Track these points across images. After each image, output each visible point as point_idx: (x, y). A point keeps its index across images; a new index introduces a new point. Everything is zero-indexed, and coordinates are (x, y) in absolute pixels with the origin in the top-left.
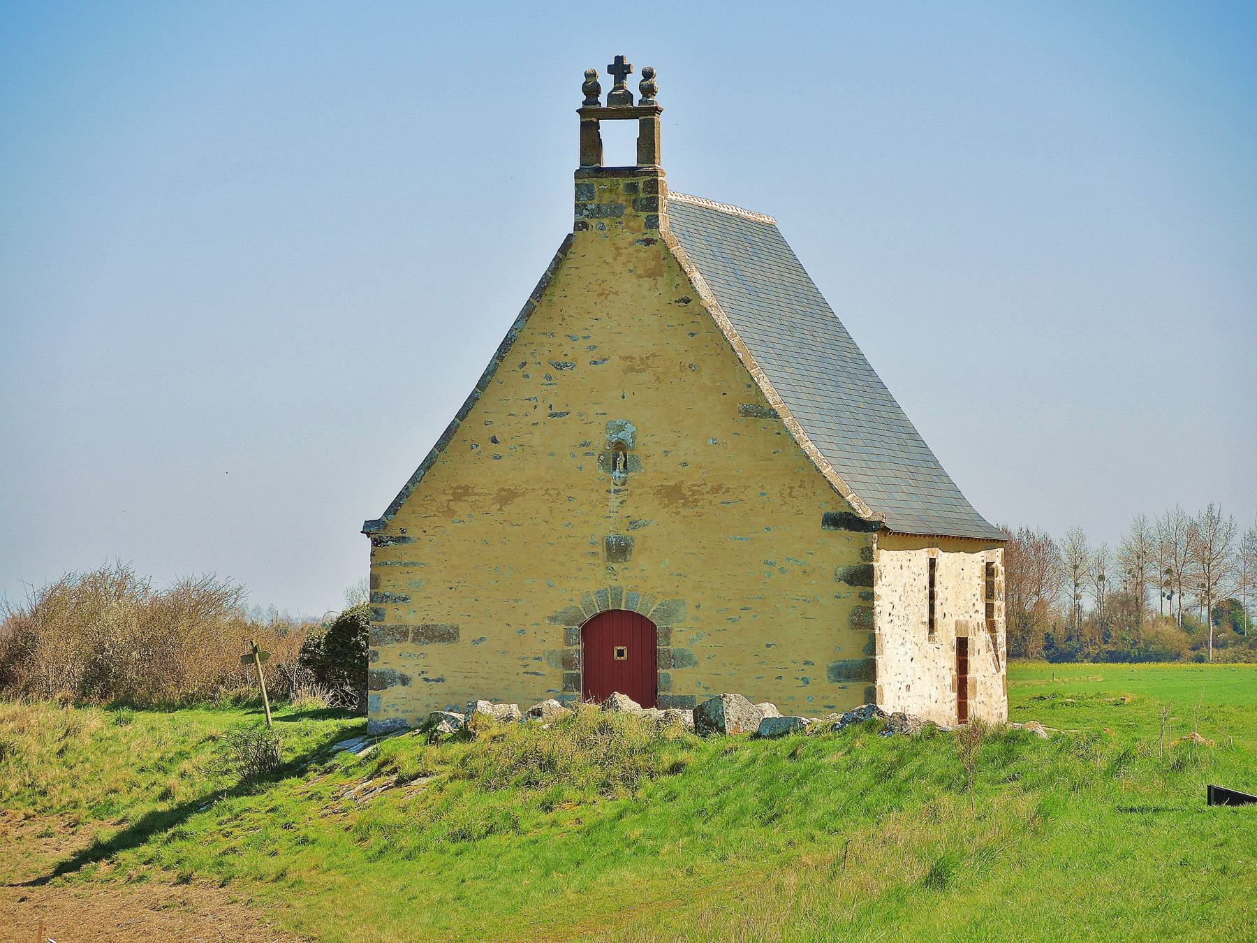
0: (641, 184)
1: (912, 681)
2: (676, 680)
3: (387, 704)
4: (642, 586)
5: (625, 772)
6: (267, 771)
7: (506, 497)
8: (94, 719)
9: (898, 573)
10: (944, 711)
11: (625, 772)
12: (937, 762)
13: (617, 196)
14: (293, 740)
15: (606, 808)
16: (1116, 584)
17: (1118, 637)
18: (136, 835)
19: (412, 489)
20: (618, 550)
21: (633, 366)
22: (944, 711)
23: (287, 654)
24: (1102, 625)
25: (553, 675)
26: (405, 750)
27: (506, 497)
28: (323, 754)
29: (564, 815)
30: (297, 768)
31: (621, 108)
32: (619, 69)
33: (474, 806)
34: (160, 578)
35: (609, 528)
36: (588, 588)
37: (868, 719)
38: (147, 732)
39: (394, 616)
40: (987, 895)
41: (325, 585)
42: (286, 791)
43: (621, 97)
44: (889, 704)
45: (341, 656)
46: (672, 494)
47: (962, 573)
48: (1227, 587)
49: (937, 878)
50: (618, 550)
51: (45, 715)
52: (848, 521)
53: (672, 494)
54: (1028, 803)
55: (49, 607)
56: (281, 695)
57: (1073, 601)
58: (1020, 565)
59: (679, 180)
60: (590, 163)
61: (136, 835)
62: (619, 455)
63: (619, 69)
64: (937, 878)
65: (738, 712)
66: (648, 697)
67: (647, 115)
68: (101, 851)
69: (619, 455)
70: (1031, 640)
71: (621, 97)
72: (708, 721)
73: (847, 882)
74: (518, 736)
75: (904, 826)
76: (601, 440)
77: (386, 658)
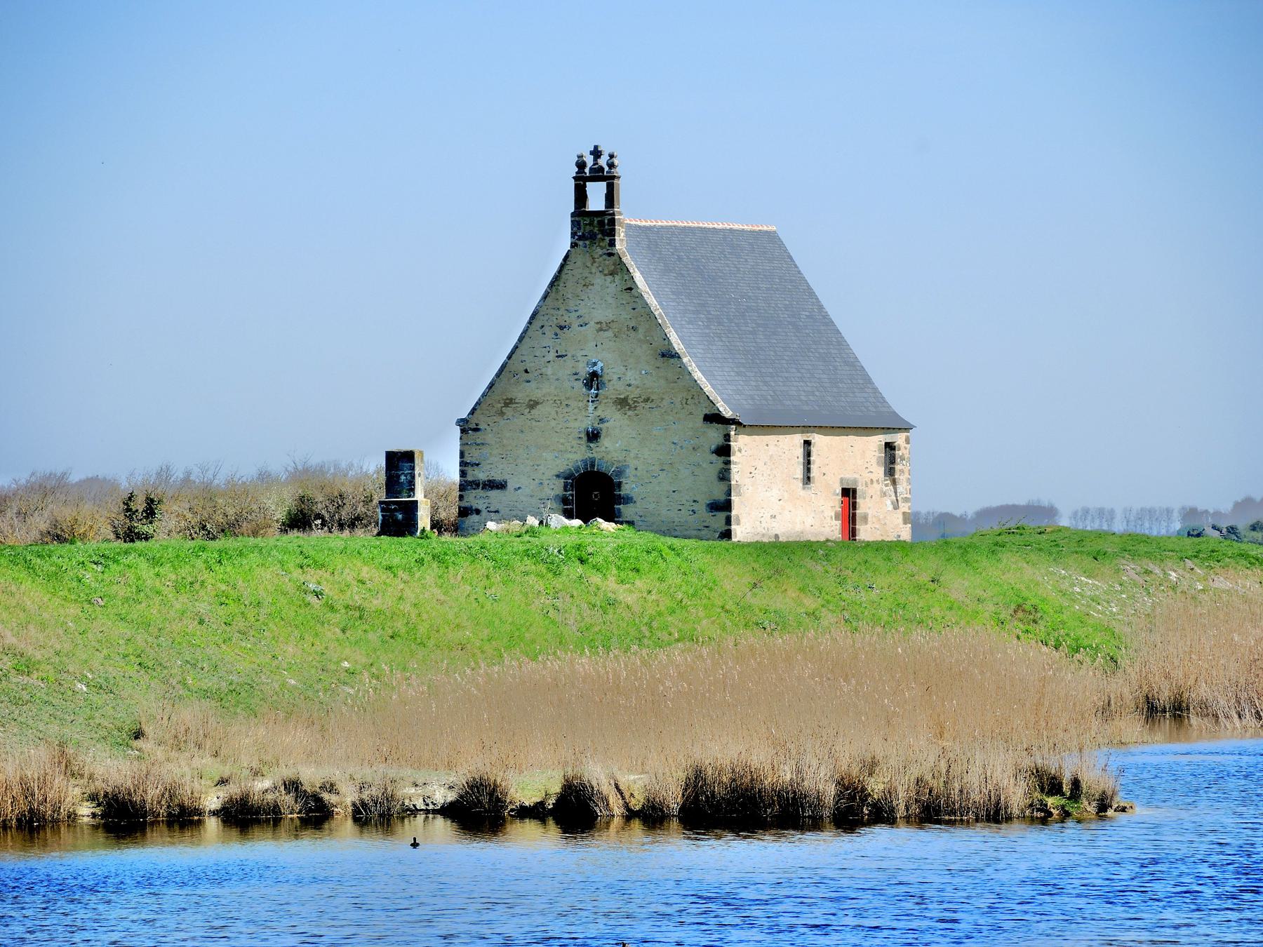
4: (609, 452)
7: (533, 405)
13: (593, 229)
21: (602, 327)
31: (598, 175)
32: (596, 153)
35: (588, 423)
36: (575, 456)
43: (594, 171)
46: (623, 403)
50: (593, 436)
52: (714, 418)
53: (623, 403)
59: (626, 216)
62: (593, 379)
63: (596, 153)
69: (593, 379)
71: (594, 171)
76: (584, 371)
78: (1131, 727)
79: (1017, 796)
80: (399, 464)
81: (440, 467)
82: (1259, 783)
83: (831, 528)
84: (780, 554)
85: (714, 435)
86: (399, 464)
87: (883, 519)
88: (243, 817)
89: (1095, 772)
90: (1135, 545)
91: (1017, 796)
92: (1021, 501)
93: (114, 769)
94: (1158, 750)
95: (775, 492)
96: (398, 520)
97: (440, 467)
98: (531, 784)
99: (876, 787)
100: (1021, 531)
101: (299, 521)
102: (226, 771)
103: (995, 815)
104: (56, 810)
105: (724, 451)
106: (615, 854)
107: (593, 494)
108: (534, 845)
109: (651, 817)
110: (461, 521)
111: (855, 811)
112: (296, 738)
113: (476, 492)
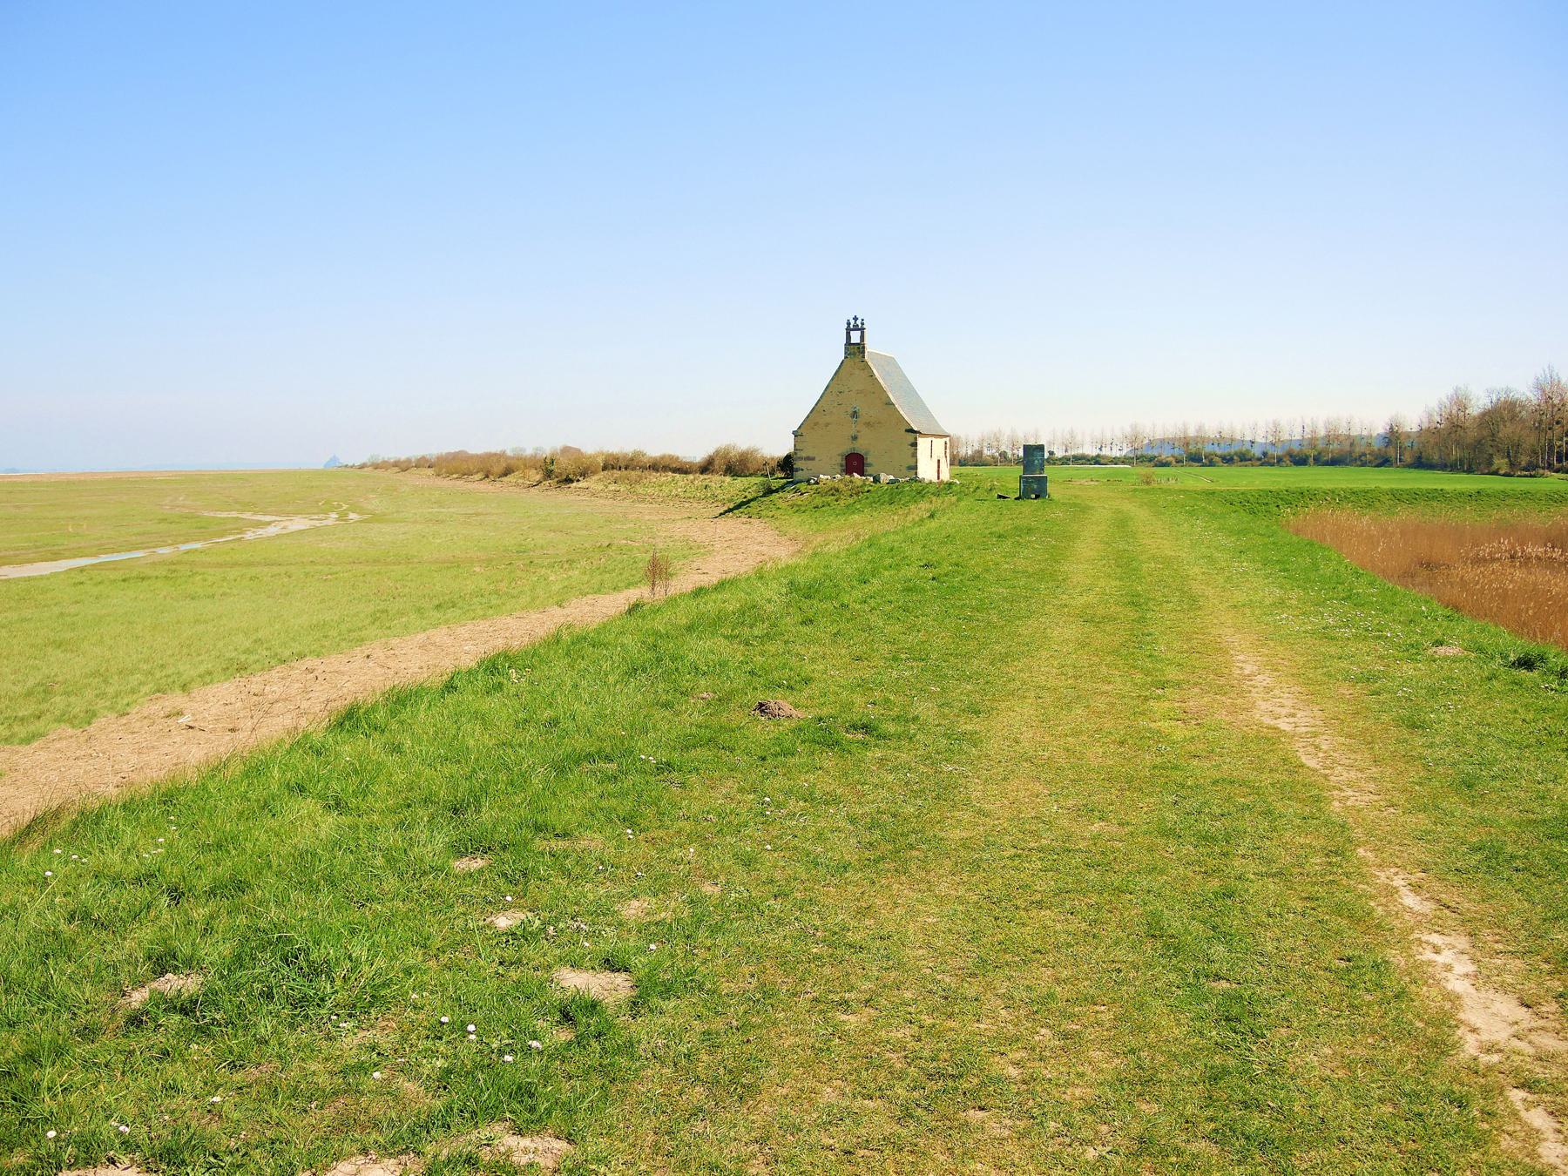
0: (860, 348)
1: (926, 471)
2: (869, 470)
3: (798, 475)
4: (860, 447)
5: (857, 492)
6: (769, 492)
7: (827, 425)
8: (728, 479)
9: (923, 443)
10: (935, 479)
11: (857, 492)
12: (932, 489)
13: (855, 350)
14: (775, 484)
15: (851, 501)
16: (976, 447)
17: (977, 460)
18: (738, 507)
19: (1408, 458)
20: (855, 438)
21: (859, 392)
22: (935, 479)
23: (774, 464)
24: (973, 457)
25: (839, 469)
26: (803, 486)
27: (827, 425)
28: (782, 488)
29: (842, 502)
30: (777, 491)
31: (856, 328)
32: (856, 319)
33: (818, 500)
34: (1480, 402)
35: (853, 433)
36: (847, 448)
37: (916, 480)
38: (741, 482)
39: (800, 454)
40: (944, 520)
41: (779, 446)
42: (774, 496)
43: (855, 326)
44: (920, 476)
45: (787, 464)
46: (868, 424)
47: (939, 444)
48: (1003, 448)
49: (932, 516)
50: (855, 438)
51: (716, 478)
52: (911, 431)
53: (868, 424)
54: (954, 499)
55: (717, 452)
56: (772, 473)
57: (966, 451)
58: (952, 443)
59: (870, 348)
60: (848, 343)
61: (738, 507)
62: (855, 414)
63: (856, 319)
64: (932, 516)
65: (885, 478)
66: (862, 474)
67: (862, 330)
68: (730, 510)
69: (855, 414)
70: (957, 461)
71: (855, 326)
72: (876, 480)
73: (910, 518)
74: (830, 484)
75: (924, 505)
76: (851, 411)
77: (798, 464)
82: (1567, 546)
85: (910, 437)
102: (1533, 648)
104: (263, 752)
105: (915, 445)
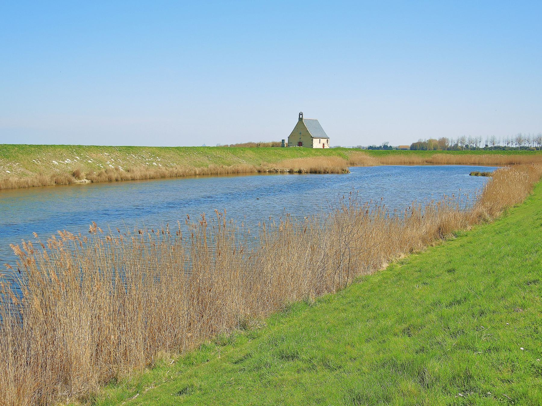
13: (301, 119)
36: (299, 141)
43: (301, 114)
59: (304, 118)
71: (301, 114)
78: (349, 165)
79: (340, 171)
80: (283, 141)
81: (286, 141)
83: (322, 147)
84: (317, 150)
86: (283, 141)
87: (326, 147)
88: (270, 172)
89: (347, 169)
90: (350, 149)
91: (340, 171)
92: (239, 143)
93: (258, 167)
94: (351, 168)
95: (317, 144)
96: (283, 146)
97: (286, 141)
98: (296, 170)
99: (327, 170)
100: (338, 148)
101: (273, 146)
103: (338, 173)
106: (304, 176)
107: (300, 144)
108: (296, 175)
109: (307, 173)
110: (288, 145)
111: (325, 172)
112: (274, 165)
113: (289, 143)
